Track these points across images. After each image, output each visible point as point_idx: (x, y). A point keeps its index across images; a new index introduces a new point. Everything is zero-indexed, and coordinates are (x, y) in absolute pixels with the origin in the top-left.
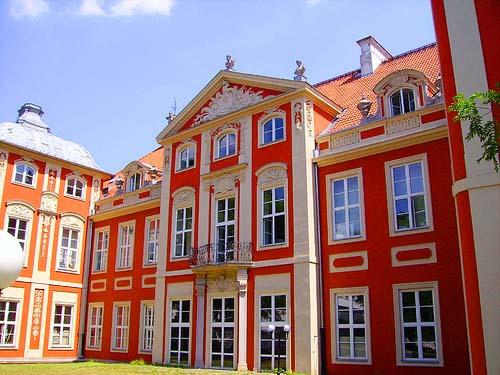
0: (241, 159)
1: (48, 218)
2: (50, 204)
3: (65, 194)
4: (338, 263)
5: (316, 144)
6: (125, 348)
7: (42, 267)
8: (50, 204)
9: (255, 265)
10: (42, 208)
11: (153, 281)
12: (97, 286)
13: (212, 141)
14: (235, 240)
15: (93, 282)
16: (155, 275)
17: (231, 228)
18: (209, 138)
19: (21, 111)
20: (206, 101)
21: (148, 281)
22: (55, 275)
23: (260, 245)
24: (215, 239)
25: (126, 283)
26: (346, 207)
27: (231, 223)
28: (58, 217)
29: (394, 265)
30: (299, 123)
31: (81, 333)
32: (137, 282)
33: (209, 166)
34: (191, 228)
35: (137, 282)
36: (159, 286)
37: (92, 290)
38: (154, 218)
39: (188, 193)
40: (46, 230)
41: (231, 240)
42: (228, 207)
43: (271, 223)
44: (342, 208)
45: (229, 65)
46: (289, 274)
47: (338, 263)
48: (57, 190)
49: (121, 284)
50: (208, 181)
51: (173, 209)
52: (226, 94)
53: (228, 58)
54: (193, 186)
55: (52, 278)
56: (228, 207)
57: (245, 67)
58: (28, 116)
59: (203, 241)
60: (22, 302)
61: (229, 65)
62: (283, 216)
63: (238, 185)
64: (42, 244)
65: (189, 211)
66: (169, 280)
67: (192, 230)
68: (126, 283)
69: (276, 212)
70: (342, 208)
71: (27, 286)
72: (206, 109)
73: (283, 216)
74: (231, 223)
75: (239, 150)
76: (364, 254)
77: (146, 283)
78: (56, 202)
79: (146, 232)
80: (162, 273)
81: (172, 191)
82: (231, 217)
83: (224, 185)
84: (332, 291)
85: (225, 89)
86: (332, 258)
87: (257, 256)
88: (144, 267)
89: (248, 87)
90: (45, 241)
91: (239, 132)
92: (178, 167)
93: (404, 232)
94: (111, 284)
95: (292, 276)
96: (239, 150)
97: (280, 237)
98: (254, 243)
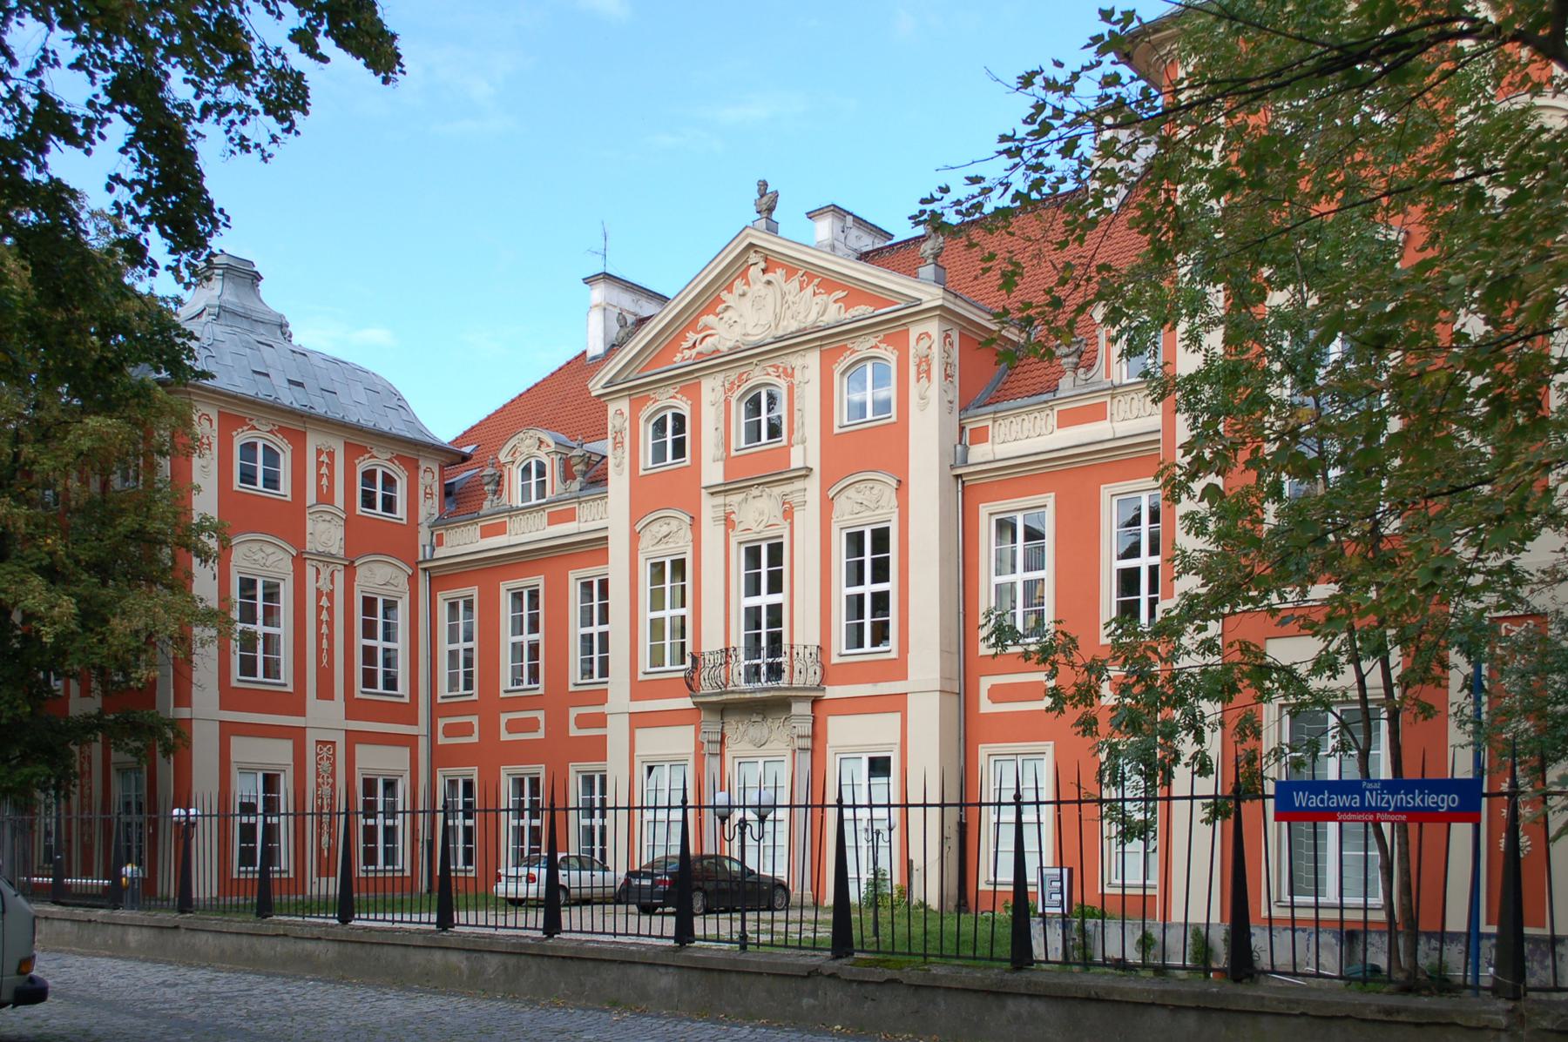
0: (796, 461)
2: (326, 534)
4: (997, 694)
6: (987, 953)
7: (325, 692)
8: (326, 534)
9: (832, 692)
11: (601, 720)
12: (450, 731)
13: (727, 403)
15: (441, 722)
16: (606, 709)
17: (775, 611)
18: (720, 395)
20: (708, 299)
21: (583, 722)
22: (354, 709)
27: (775, 599)
28: (350, 570)
29: (982, 710)
30: (924, 381)
33: (721, 465)
34: (1041, 566)
36: (616, 732)
37: (441, 740)
38: (593, 573)
39: (674, 523)
40: (324, 602)
41: (775, 639)
42: (766, 563)
43: (591, 641)
46: (898, 715)
47: (997, 694)
49: (513, 726)
50: (720, 500)
52: (758, 287)
53: (763, 185)
54: (891, 473)
55: (349, 716)
56: (766, 563)
59: (712, 642)
60: (407, 775)
61: (767, 204)
62: (887, 593)
63: (788, 514)
66: (639, 721)
67: (687, 611)
71: (297, 736)
72: (709, 319)
73: (887, 593)
74: (775, 599)
75: (791, 431)
77: (446, 736)
80: (619, 698)
81: (634, 518)
82: (775, 585)
84: (983, 751)
86: (986, 683)
88: (571, 688)
90: (324, 629)
91: (791, 389)
92: (646, 459)
94: (490, 728)
95: (902, 486)
98: (823, 649)
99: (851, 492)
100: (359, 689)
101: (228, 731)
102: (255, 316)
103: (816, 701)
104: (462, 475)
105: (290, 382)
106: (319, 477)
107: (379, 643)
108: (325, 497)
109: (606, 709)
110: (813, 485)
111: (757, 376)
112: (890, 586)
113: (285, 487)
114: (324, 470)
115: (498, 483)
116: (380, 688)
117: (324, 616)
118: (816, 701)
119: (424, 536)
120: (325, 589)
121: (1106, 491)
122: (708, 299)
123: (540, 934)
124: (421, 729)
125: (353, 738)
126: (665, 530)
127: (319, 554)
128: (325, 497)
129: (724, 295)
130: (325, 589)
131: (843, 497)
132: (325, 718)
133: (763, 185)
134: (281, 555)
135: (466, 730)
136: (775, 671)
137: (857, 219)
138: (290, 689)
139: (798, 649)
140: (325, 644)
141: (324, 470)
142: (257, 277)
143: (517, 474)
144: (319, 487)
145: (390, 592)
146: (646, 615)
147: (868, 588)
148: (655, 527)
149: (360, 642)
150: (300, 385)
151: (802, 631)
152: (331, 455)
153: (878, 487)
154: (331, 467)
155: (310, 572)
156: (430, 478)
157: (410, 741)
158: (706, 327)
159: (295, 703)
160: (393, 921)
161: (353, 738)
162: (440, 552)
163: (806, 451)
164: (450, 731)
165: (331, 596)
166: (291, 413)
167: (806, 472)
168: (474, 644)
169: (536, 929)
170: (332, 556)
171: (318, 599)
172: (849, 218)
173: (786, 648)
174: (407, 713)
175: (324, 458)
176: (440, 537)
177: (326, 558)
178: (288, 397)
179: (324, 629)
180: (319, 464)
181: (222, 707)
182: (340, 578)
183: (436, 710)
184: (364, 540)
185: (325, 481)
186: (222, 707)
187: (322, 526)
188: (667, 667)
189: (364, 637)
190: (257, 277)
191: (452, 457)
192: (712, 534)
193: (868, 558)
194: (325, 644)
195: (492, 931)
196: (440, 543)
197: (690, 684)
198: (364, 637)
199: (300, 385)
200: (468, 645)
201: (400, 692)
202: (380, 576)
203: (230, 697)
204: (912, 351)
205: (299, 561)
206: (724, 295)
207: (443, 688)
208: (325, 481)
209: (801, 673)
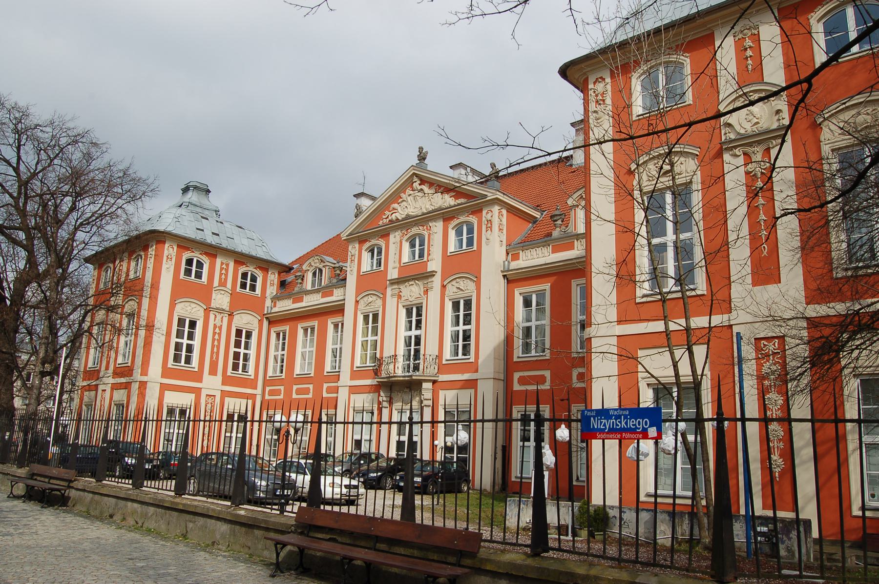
1: (219, 316)
2: (221, 300)
3: (238, 289)
5: (508, 254)
7: (213, 372)
8: (221, 300)
9: (442, 378)
10: (213, 305)
11: (336, 390)
12: (271, 393)
14: (422, 352)
15: (268, 389)
18: (398, 239)
19: (186, 190)
20: (395, 196)
22: (226, 380)
23: (447, 354)
24: (401, 349)
25: (307, 391)
26: (308, 349)
27: (418, 332)
28: (231, 315)
30: (489, 232)
31: (500, 443)
32: (318, 390)
35: (318, 390)
36: (343, 395)
37: (267, 397)
38: (337, 319)
39: (375, 298)
40: (217, 330)
41: (417, 352)
42: (415, 314)
44: (543, 322)
45: (422, 157)
46: (473, 391)
47: (523, 381)
48: (229, 285)
49: (299, 392)
51: (447, 299)
53: (421, 149)
55: (223, 384)
56: (415, 314)
57: (439, 165)
58: (192, 196)
59: (388, 352)
61: (422, 157)
63: (426, 292)
64: (213, 346)
65: (376, 317)
67: (378, 338)
68: (307, 391)
69: (464, 324)
70: (543, 322)
71: (197, 391)
72: (395, 205)
74: (418, 332)
75: (429, 255)
76: (547, 374)
78: (228, 299)
79: (573, 307)
80: (345, 379)
82: (418, 327)
83: (412, 292)
85: (416, 185)
86: (517, 376)
87: (443, 368)
89: (440, 187)
90: (216, 343)
91: (429, 235)
93: (527, 357)
94: (288, 392)
96: (429, 255)
97: (466, 350)
98: (440, 356)
99: (454, 283)
100: (171, 363)
101: (164, 388)
102: (205, 206)
103: (434, 382)
104: (290, 278)
105: (213, 233)
106: (221, 274)
107: (242, 351)
108: (223, 283)
109: (339, 384)
110: (437, 281)
111: (415, 230)
112: (472, 327)
113: (258, 290)
114: (224, 271)
115: (302, 280)
116: (240, 371)
117: (217, 337)
118: (434, 382)
119: (268, 303)
120: (218, 325)
121: (574, 283)
122: (395, 196)
123: (173, 494)
124: (259, 391)
125: (224, 394)
126: (370, 299)
127: (217, 309)
128: (223, 283)
129: (402, 195)
130: (218, 325)
131: (449, 285)
132: (212, 384)
133: (421, 149)
134: (199, 308)
135: (278, 392)
136: (416, 368)
137: (472, 169)
138: (196, 370)
139: (428, 357)
140: (215, 350)
141: (224, 271)
142: (208, 191)
143: (310, 275)
144: (220, 279)
145: (249, 327)
146: (174, 340)
147: (461, 327)
148: (366, 299)
149: (232, 349)
150: (218, 235)
151: (430, 348)
152: (227, 265)
153: (193, 305)
154: (227, 270)
155: (212, 316)
156: (273, 277)
157: (253, 397)
158: (394, 209)
159: (198, 376)
160: (118, 482)
161: (224, 394)
162: (275, 310)
163: (435, 264)
164: (271, 393)
165: (220, 328)
166: (210, 246)
167: (432, 274)
168: (285, 352)
169: (170, 490)
170: (223, 310)
171: (215, 329)
172: (469, 169)
173: (421, 356)
174: (253, 384)
175: (224, 266)
176: (275, 303)
177: (220, 311)
178: (211, 239)
179: (216, 343)
180: (222, 269)
181: (223, 384)
182: (226, 320)
183: (266, 383)
184: (238, 304)
185: (223, 276)
186: (223, 384)
187: (220, 296)
188: (368, 364)
189: (177, 337)
190: (208, 191)
191: (288, 269)
192: (391, 302)
193: (461, 313)
194: (215, 350)
195: (156, 491)
196: (275, 306)
197: (376, 372)
198: (177, 337)
199: (218, 235)
200: (283, 353)
201: (193, 366)
202: (245, 320)
203: (166, 372)
204: (484, 219)
205: (207, 311)
206: (402, 195)
207: (270, 373)
208: (223, 276)
209: (428, 369)
